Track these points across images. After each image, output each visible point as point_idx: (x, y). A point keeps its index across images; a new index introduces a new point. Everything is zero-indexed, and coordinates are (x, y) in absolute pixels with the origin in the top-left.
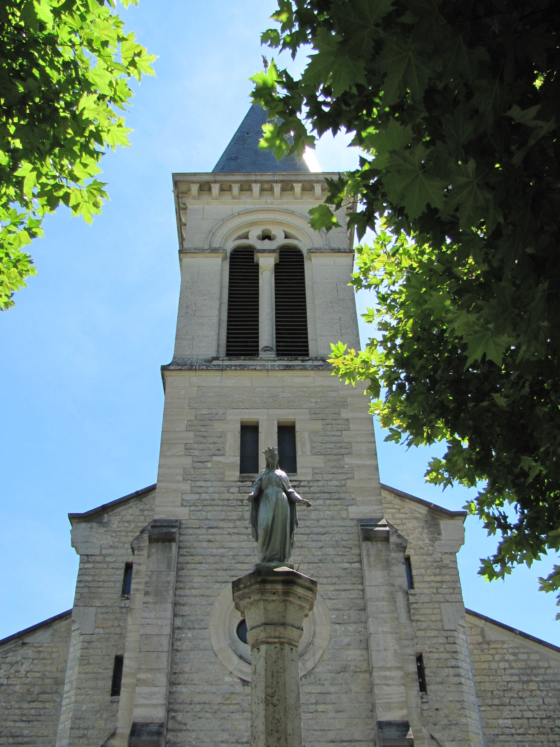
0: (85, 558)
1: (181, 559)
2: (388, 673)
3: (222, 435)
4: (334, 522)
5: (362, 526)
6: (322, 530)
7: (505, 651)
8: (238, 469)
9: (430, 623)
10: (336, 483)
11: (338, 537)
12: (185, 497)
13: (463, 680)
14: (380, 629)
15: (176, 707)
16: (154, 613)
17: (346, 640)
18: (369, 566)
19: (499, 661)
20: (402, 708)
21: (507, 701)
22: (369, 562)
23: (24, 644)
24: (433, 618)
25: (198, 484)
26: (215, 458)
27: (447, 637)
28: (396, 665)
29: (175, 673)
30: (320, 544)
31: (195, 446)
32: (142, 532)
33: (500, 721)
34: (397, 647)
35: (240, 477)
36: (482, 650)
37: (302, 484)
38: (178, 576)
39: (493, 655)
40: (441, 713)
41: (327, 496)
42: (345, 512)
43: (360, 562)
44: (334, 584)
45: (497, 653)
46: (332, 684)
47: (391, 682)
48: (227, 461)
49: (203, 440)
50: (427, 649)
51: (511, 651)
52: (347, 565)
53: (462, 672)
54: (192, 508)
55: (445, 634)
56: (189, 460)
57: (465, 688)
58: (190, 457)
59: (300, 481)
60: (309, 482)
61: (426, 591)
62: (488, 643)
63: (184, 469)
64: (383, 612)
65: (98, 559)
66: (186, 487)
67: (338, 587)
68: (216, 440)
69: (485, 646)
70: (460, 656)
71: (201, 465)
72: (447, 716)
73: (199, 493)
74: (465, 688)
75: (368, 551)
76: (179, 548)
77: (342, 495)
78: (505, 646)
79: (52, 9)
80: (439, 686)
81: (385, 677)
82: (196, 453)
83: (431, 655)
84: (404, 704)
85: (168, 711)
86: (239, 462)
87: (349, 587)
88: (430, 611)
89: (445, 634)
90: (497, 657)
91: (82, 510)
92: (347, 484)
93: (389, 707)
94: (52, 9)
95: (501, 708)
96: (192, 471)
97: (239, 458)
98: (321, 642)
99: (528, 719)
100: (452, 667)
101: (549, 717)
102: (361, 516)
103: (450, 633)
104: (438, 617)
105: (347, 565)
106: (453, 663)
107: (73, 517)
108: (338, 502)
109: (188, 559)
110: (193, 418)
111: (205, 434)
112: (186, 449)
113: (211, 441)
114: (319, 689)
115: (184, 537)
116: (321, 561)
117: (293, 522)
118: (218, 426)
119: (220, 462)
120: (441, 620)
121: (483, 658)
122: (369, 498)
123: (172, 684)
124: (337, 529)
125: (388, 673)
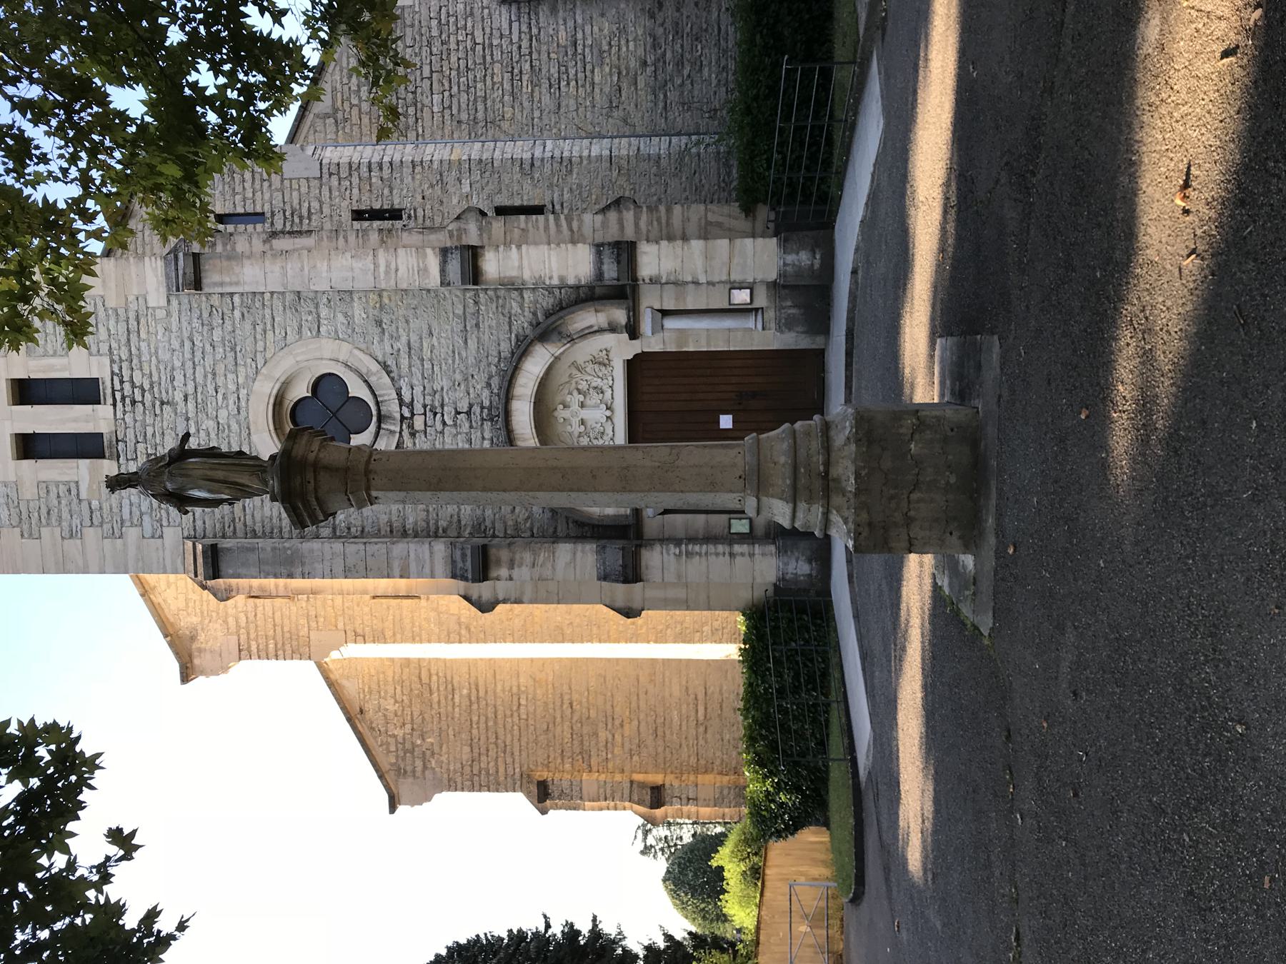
0: (243, 653)
1: (240, 533)
2: (382, 269)
3: (46, 486)
4: (174, 328)
5: (178, 290)
6: (187, 344)
7: (346, 88)
8: (100, 461)
9: (312, 195)
10: (112, 323)
11: (196, 323)
12: (148, 533)
13: (386, 159)
14: (324, 274)
15: (432, 528)
16: (316, 565)
17: (340, 317)
18: (237, 284)
19: (360, 98)
20: (425, 256)
21: (410, 96)
22: (231, 284)
23: (361, 711)
24: (304, 189)
25: (126, 516)
26: (83, 495)
27: (331, 174)
28: (371, 257)
29: (391, 531)
30: (208, 347)
31: (64, 524)
32: (204, 587)
33: (436, 109)
34: (348, 255)
35: (111, 458)
36: (346, 120)
37: (117, 371)
38: (264, 536)
39: (352, 106)
40: (428, 193)
41: (134, 337)
42: (158, 311)
43: (232, 294)
44: (265, 331)
45: (349, 99)
46: (398, 338)
47: (393, 266)
48: (87, 478)
49: (54, 513)
50: (347, 202)
51: (345, 81)
52: (237, 313)
53: (376, 159)
54: (165, 523)
55: (326, 176)
56: (90, 534)
57: (397, 158)
58: (85, 530)
59: (113, 373)
60: (112, 361)
61: (267, 196)
62: (336, 110)
63: (103, 538)
64: (302, 270)
65: (243, 637)
66: (132, 533)
67: (269, 327)
68: (53, 495)
69: (340, 115)
70: (355, 160)
71: (97, 515)
72: (432, 186)
73: (142, 514)
74: (397, 158)
75: (215, 284)
76: (224, 537)
77: (132, 315)
78: (339, 86)
79: (165, 925)
80: (395, 192)
81: (387, 272)
82: (76, 521)
83: (355, 198)
84: (420, 249)
85: (436, 536)
86: (88, 461)
87: (268, 311)
88: (295, 194)
89: (326, 176)
90: (355, 101)
91: (174, 667)
92: (113, 305)
93: (424, 271)
94: (165, 925)
95: (419, 105)
96: (107, 527)
97: (81, 461)
98: (344, 352)
99: (432, 72)
100: (370, 171)
101: (429, 45)
102: (163, 290)
103: (325, 170)
104: (303, 182)
105: (237, 313)
106: (364, 169)
107: (185, 678)
108: (143, 321)
109: (239, 526)
110: (18, 530)
111: (44, 511)
112: (71, 537)
113: (55, 502)
114: (404, 355)
115: (207, 532)
116: (233, 349)
117: (212, 453)
118: (29, 492)
119: (90, 486)
120: (307, 179)
121: (355, 119)
122: (134, 276)
123: (404, 534)
124: (185, 324)
125: (382, 269)
